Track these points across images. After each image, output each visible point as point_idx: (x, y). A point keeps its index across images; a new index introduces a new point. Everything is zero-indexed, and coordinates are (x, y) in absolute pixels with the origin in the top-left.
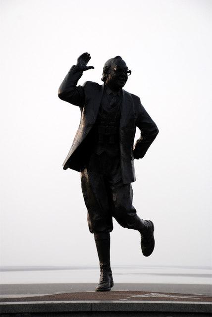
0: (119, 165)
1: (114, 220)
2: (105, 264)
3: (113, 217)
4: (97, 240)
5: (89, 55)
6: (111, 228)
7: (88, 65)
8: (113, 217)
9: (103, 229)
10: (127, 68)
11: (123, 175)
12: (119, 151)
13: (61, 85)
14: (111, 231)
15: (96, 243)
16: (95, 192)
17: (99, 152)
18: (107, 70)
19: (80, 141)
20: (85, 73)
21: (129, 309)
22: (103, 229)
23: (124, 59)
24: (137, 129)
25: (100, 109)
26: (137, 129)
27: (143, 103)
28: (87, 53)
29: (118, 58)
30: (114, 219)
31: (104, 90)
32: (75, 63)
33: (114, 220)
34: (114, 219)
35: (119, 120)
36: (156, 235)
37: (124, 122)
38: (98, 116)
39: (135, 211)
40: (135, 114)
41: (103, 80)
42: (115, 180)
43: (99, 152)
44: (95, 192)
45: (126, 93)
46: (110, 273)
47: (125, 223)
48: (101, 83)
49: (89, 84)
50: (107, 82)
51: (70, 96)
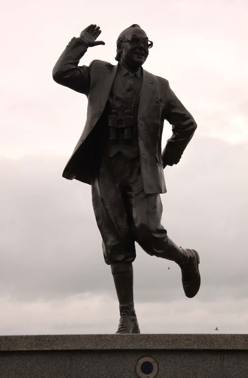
0: (139, 172)
1: (137, 246)
2: (125, 306)
3: (135, 242)
4: (115, 273)
5: (99, 28)
6: (133, 256)
7: (98, 39)
8: (135, 242)
9: (121, 258)
10: (147, 38)
11: (145, 183)
12: (138, 151)
13: (57, 62)
14: (133, 260)
15: (114, 276)
16: (108, 207)
17: (113, 152)
18: (121, 42)
19: (85, 138)
20: (90, 49)
21: (71, 347)
22: (121, 258)
23: (143, 27)
24: (166, 123)
25: (111, 94)
26: (166, 123)
27: (173, 87)
28: (95, 26)
29: (134, 26)
30: (136, 244)
31: (118, 71)
32: (78, 36)
33: (137, 246)
34: (136, 244)
35: (137, 106)
36: (202, 269)
37: (143, 110)
38: (108, 103)
39: (165, 232)
40: (161, 100)
41: (118, 58)
42: (135, 189)
43: (113, 152)
44: (108, 207)
45: (150, 76)
46: (132, 318)
47: (150, 250)
48: (115, 63)
49: (96, 64)
50: (121, 60)
51: (68, 76)
